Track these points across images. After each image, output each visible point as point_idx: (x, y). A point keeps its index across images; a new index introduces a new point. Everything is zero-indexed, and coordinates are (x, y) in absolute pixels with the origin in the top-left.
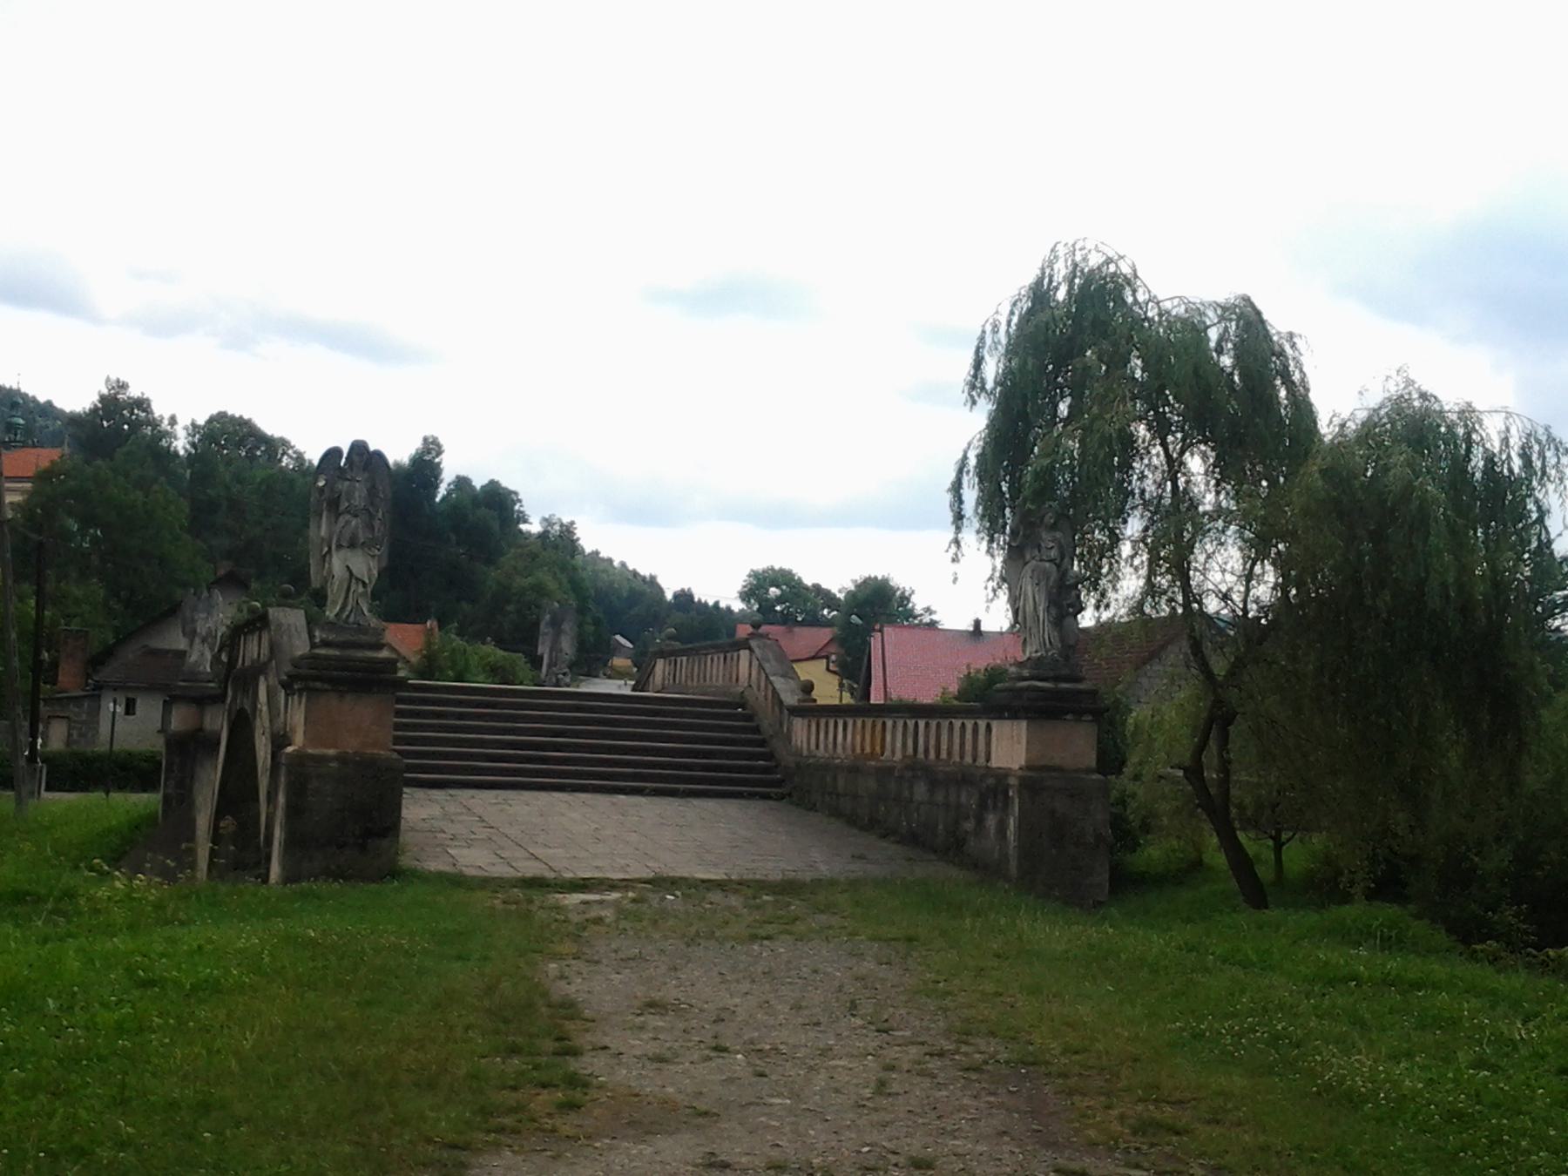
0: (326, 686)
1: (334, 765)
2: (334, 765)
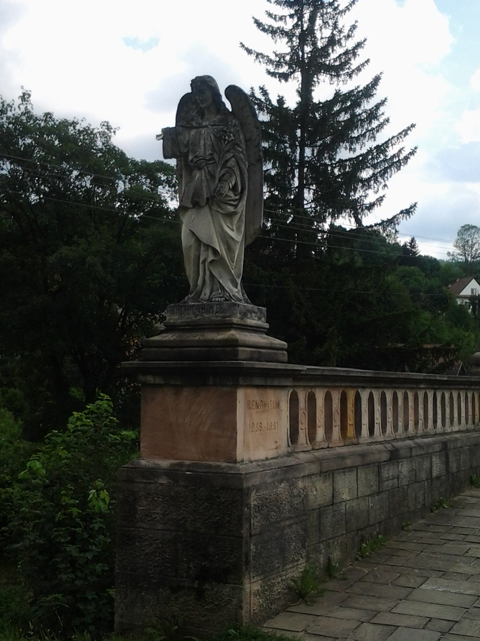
0: (159, 380)
1: (163, 480)
2: (163, 480)
